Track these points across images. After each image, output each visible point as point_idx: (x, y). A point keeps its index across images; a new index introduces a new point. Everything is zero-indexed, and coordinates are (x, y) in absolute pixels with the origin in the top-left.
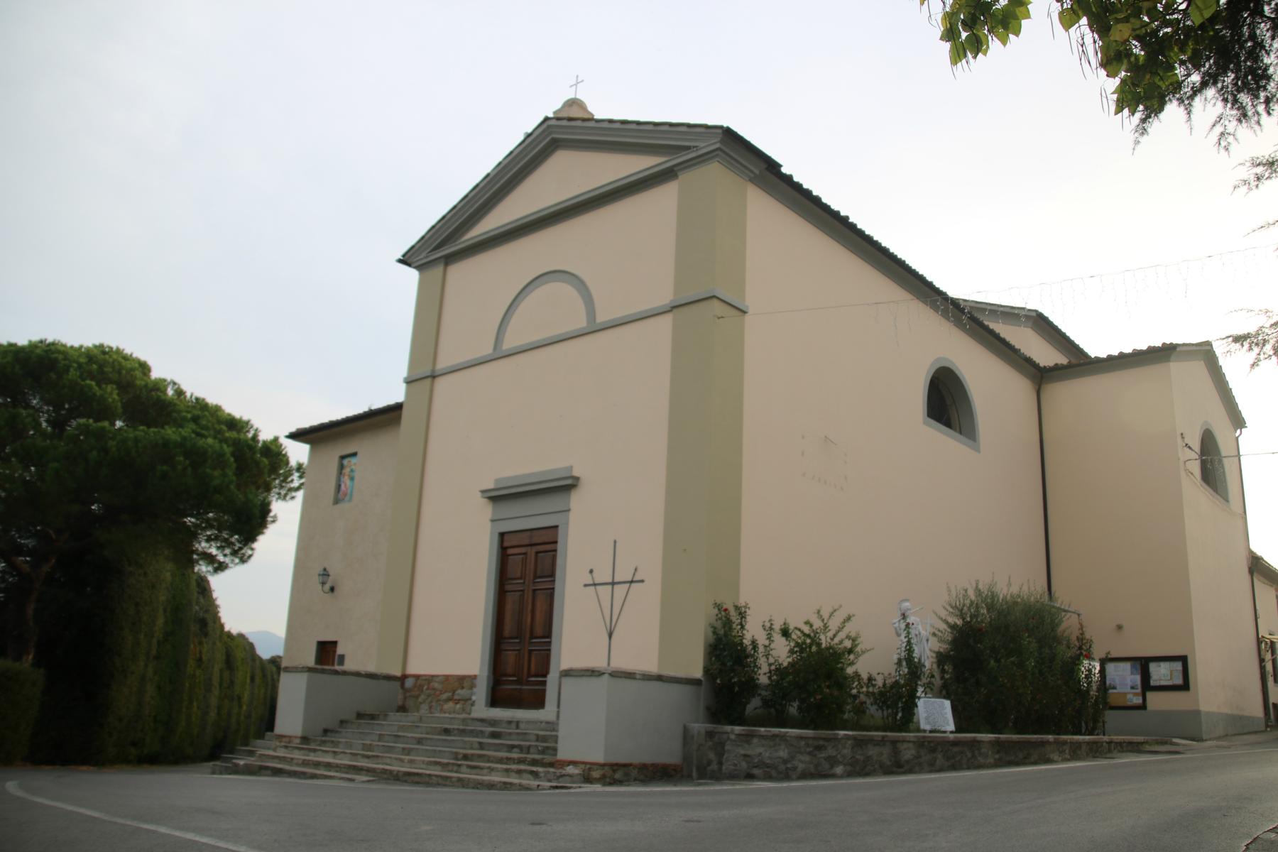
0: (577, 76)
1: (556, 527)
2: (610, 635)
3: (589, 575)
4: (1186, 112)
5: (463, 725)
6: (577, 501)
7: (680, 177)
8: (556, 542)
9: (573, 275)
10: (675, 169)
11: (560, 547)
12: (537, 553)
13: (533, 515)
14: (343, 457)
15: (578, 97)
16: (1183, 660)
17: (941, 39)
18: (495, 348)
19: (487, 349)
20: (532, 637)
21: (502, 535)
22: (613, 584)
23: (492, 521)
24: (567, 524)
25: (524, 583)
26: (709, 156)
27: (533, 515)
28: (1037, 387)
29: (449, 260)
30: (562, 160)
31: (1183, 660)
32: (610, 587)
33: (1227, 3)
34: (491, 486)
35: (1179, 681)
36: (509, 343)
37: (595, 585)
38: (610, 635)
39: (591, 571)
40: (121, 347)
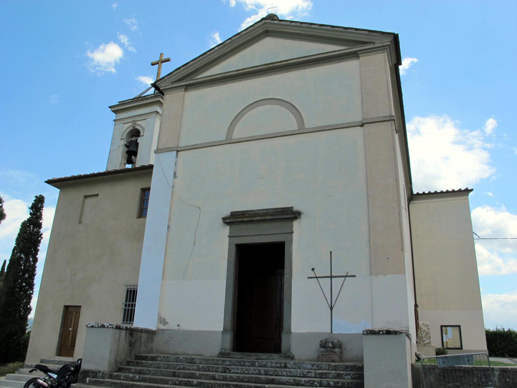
1: (80, 307)
2: (331, 308)
3: (313, 272)
4: (139, 140)
5: (469, 365)
7: (361, 58)
10: (358, 53)
14: (86, 197)
17: (398, 34)
19: (222, 137)
20: (76, 312)
22: (331, 277)
23: (229, 236)
24: (291, 241)
26: (370, 50)
28: (408, 202)
29: (187, 87)
30: (268, 42)
32: (329, 279)
35: (460, 347)
36: (236, 136)
37: (317, 277)
38: (331, 308)
39: (313, 269)
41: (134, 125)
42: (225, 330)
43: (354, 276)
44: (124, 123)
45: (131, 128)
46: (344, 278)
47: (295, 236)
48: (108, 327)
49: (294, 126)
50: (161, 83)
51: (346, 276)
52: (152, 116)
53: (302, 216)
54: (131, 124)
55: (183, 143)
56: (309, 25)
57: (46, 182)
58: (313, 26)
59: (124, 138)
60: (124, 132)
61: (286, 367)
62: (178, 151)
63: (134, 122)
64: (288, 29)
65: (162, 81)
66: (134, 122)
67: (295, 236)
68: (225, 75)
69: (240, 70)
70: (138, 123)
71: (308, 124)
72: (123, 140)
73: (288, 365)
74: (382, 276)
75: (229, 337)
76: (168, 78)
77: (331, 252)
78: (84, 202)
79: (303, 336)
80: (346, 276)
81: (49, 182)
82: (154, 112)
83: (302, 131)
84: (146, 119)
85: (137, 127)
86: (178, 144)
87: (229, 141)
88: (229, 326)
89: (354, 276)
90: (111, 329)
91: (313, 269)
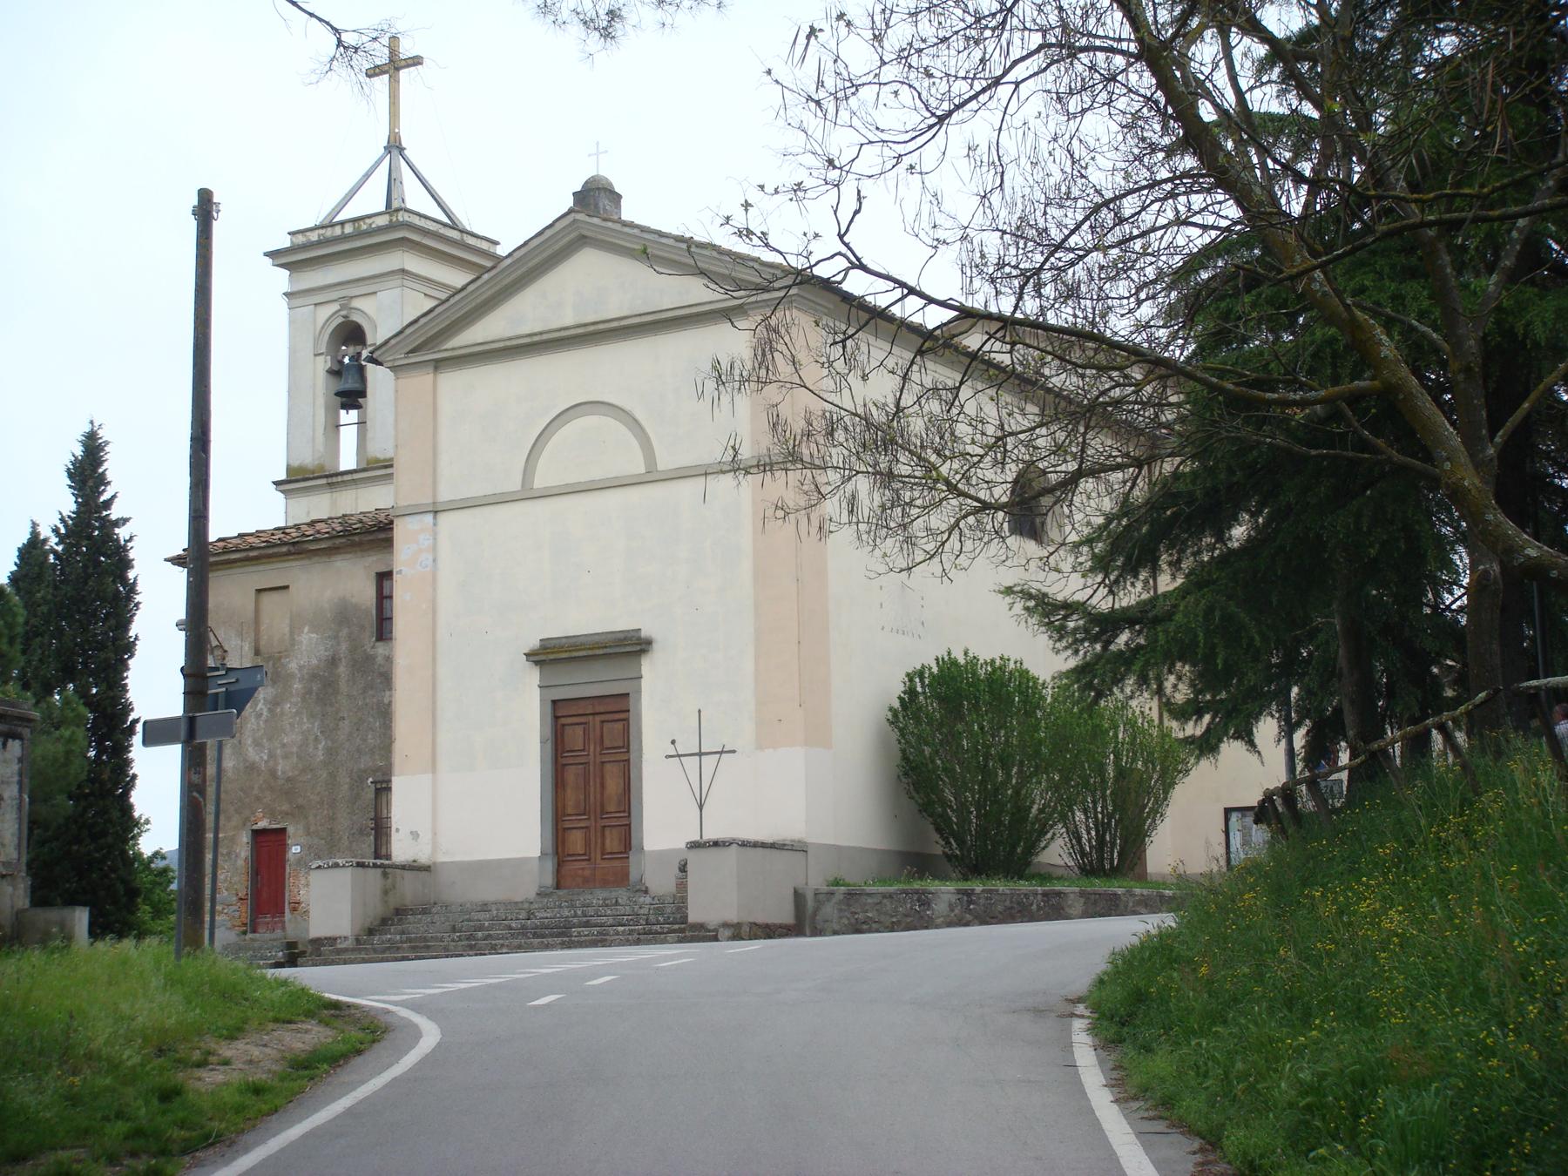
0: (598, 143)
1: (628, 694)
2: (701, 807)
6: (649, 668)
8: (628, 711)
9: (617, 407)
11: (632, 715)
12: (603, 722)
13: (369, 294)
15: (601, 173)
16: (1228, 812)
18: (523, 486)
21: (554, 702)
24: (639, 691)
25: (588, 755)
27: (369, 294)
29: (438, 365)
31: (1228, 812)
32: (698, 758)
33: (1345, 5)
34: (286, 242)
36: (539, 482)
37: (679, 756)
38: (701, 807)
39: (673, 742)
40: (140, 648)
41: (343, 313)
42: (543, 853)
43: (734, 752)
44: (316, 305)
45: (340, 320)
46: (718, 756)
47: (645, 684)
48: (344, 866)
49: (639, 467)
50: (382, 354)
51: (721, 753)
52: (391, 284)
53: (655, 646)
54: (335, 307)
55: (445, 495)
56: (656, 236)
57: (130, 518)
58: (664, 240)
59: (323, 350)
60: (321, 332)
61: (617, 903)
62: (436, 512)
63: (345, 303)
64: (619, 238)
65: (384, 349)
66: (345, 303)
67: (645, 683)
68: (508, 343)
69: (535, 334)
70: (356, 303)
71: (666, 461)
72: (322, 358)
73: (620, 901)
74: (771, 750)
75: (550, 865)
76: (397, 343)
77: (699, 711)
78: (257, 602)
79: (662, 855)
80: (721, 753)
81: (166, 560)
82: (393, 273)
83: (651, 477)
84: (375, 293)
85: (356, 318)
86: (434, 495)
87: (528, 494)
88: (550, 849)
89: (734, 752)
90: (350, 868)
91: (673, 742)
